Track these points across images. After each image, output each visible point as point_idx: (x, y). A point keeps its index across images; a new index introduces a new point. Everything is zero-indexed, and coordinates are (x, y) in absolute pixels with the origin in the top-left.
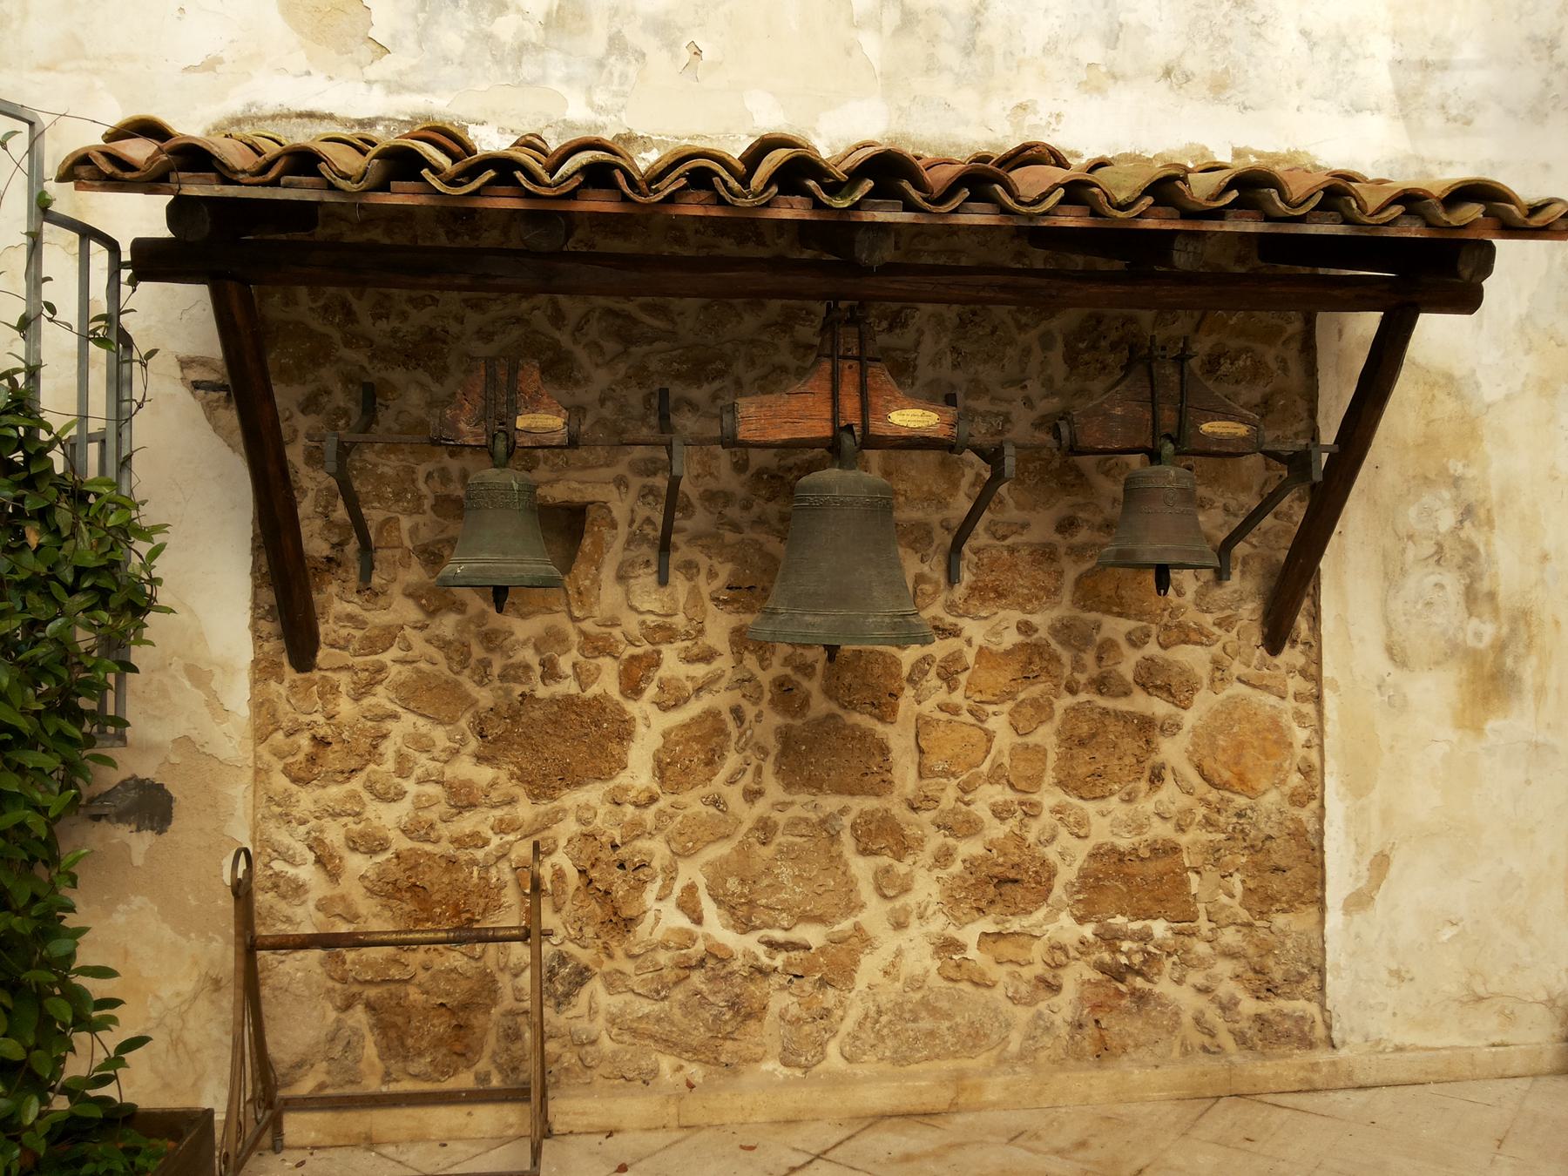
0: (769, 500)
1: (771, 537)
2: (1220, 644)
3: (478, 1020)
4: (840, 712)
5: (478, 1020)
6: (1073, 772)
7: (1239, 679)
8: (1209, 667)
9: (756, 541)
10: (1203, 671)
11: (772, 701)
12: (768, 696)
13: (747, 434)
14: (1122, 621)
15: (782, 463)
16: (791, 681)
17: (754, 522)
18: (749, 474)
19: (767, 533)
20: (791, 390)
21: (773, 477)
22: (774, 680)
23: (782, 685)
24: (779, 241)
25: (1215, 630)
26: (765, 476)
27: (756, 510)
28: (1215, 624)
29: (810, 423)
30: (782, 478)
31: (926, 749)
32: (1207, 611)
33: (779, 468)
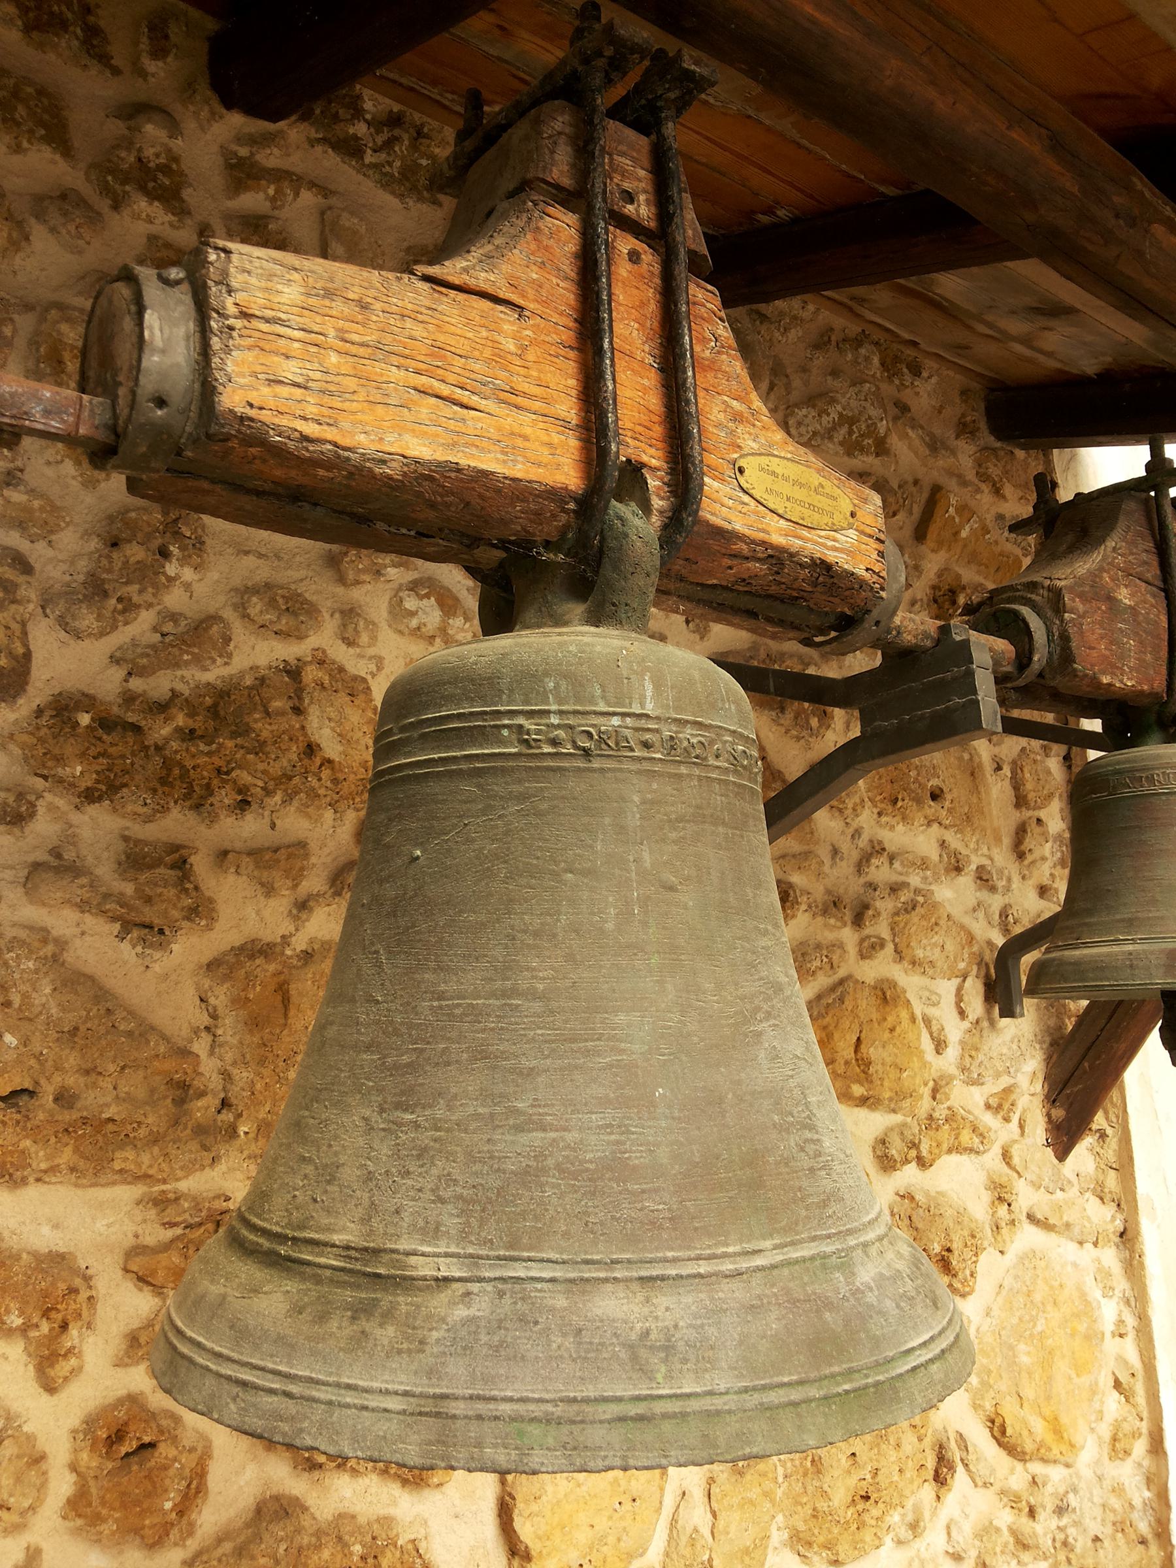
0: (90, 796)
1: (89, 920)
2: (996, 1150)
3: (69, 42)
4: (295, 1484)
5: (69, 42)
6: (822, 1505)
7: (1030, 1217)
8: (987, 1197)
9: (44, 934)
10: (979, 1207)
11: (77, 1505)
12: (62, 1485)
13: (264, 394)
14: (862, 1113)
15: (136, 684)
16: (151, 1416)
17: (36, 866)
18: (25, 706)
19: (83, 906)
20: (451, 269)
21: (106, 723)
22: (90, 1423)
23: (118, 1436)
24: (152, 66)
25: (989, 1120)
26: (85, 719)
27: (43, 827)
28: (988, 1106)
29: (511, 420)
30: (136, 729)
31: (534, 1546)
32: (977, 1082)
33: (129, 698)
